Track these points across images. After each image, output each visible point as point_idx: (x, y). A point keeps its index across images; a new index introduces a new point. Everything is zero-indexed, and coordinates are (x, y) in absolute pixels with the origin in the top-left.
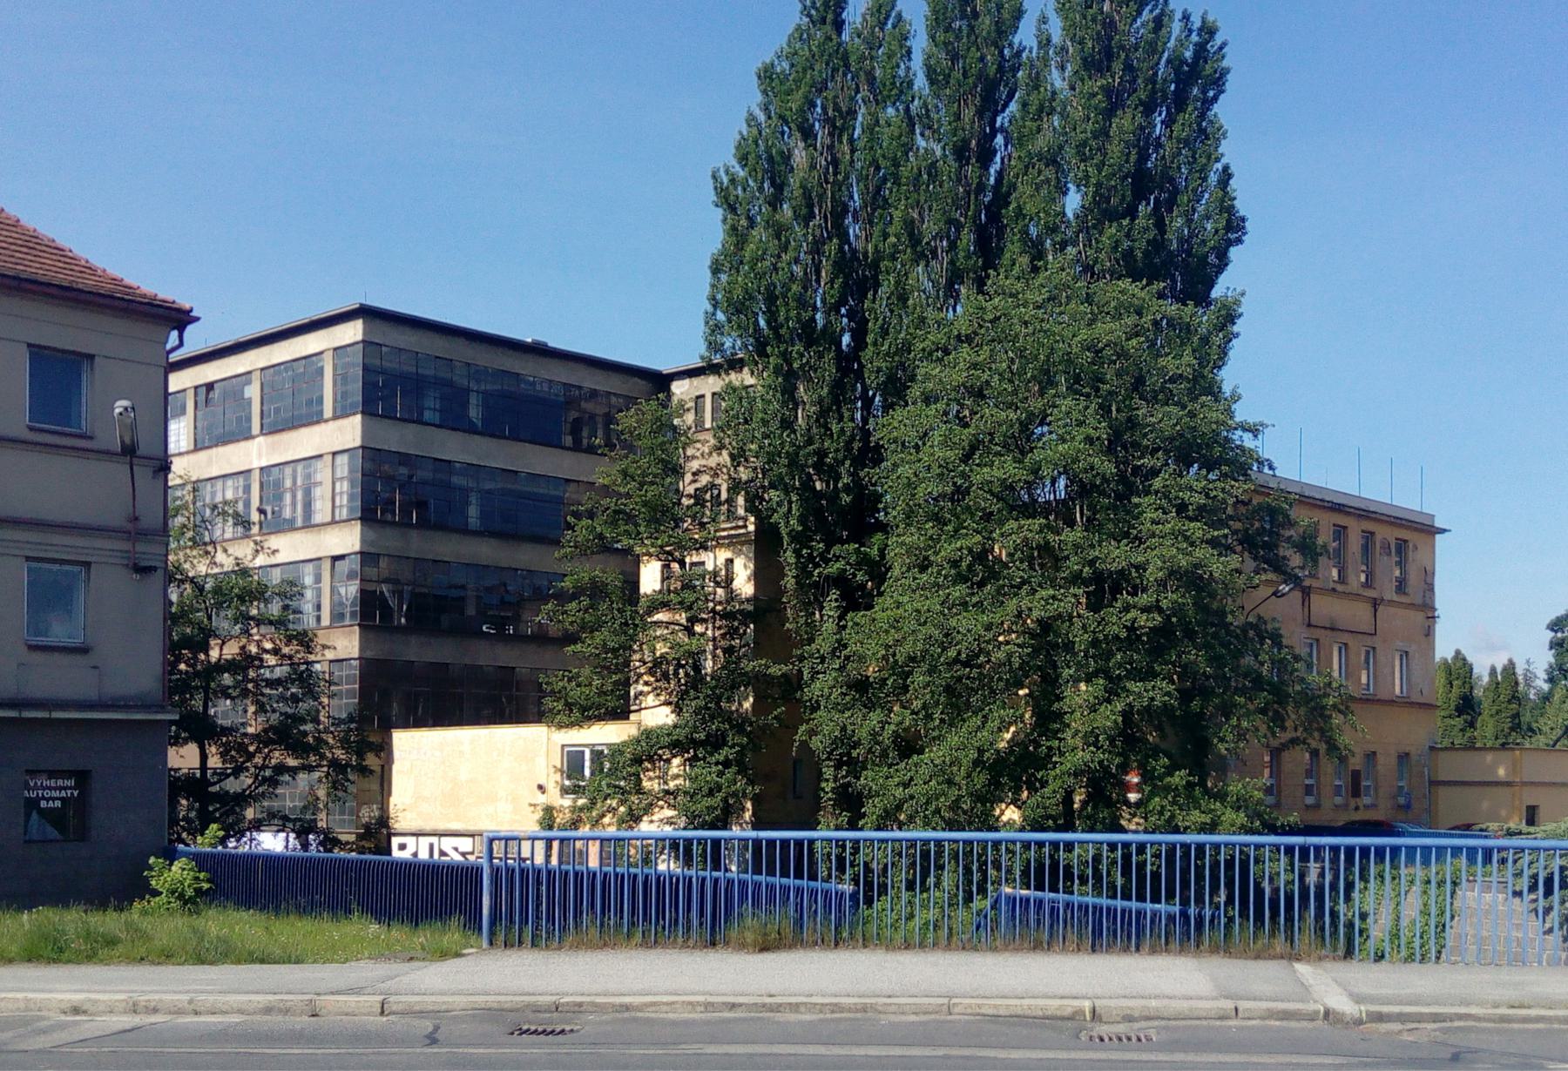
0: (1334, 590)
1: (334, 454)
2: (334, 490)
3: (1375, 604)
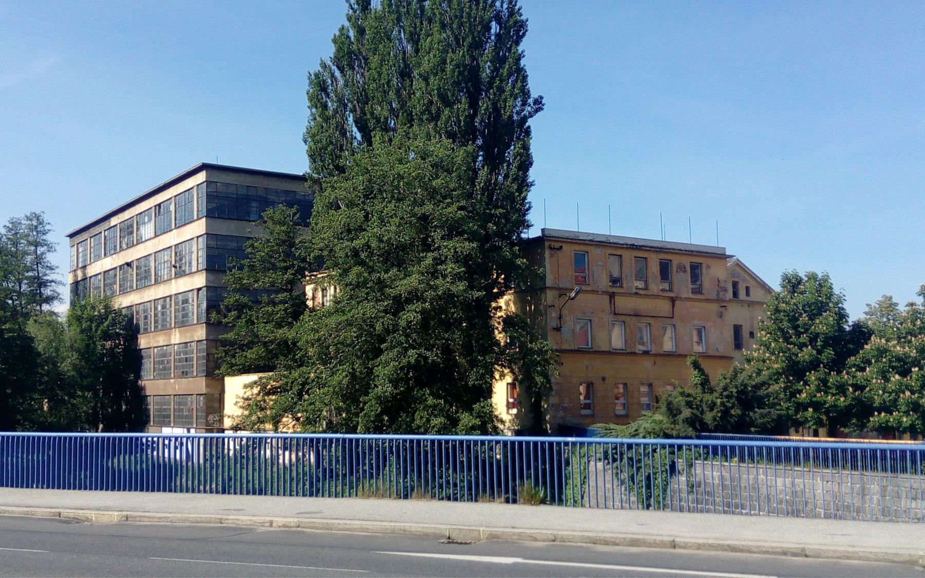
0: (636, 293)
1: (198, 237)
2: (197, 256)
3: (673, 301)
